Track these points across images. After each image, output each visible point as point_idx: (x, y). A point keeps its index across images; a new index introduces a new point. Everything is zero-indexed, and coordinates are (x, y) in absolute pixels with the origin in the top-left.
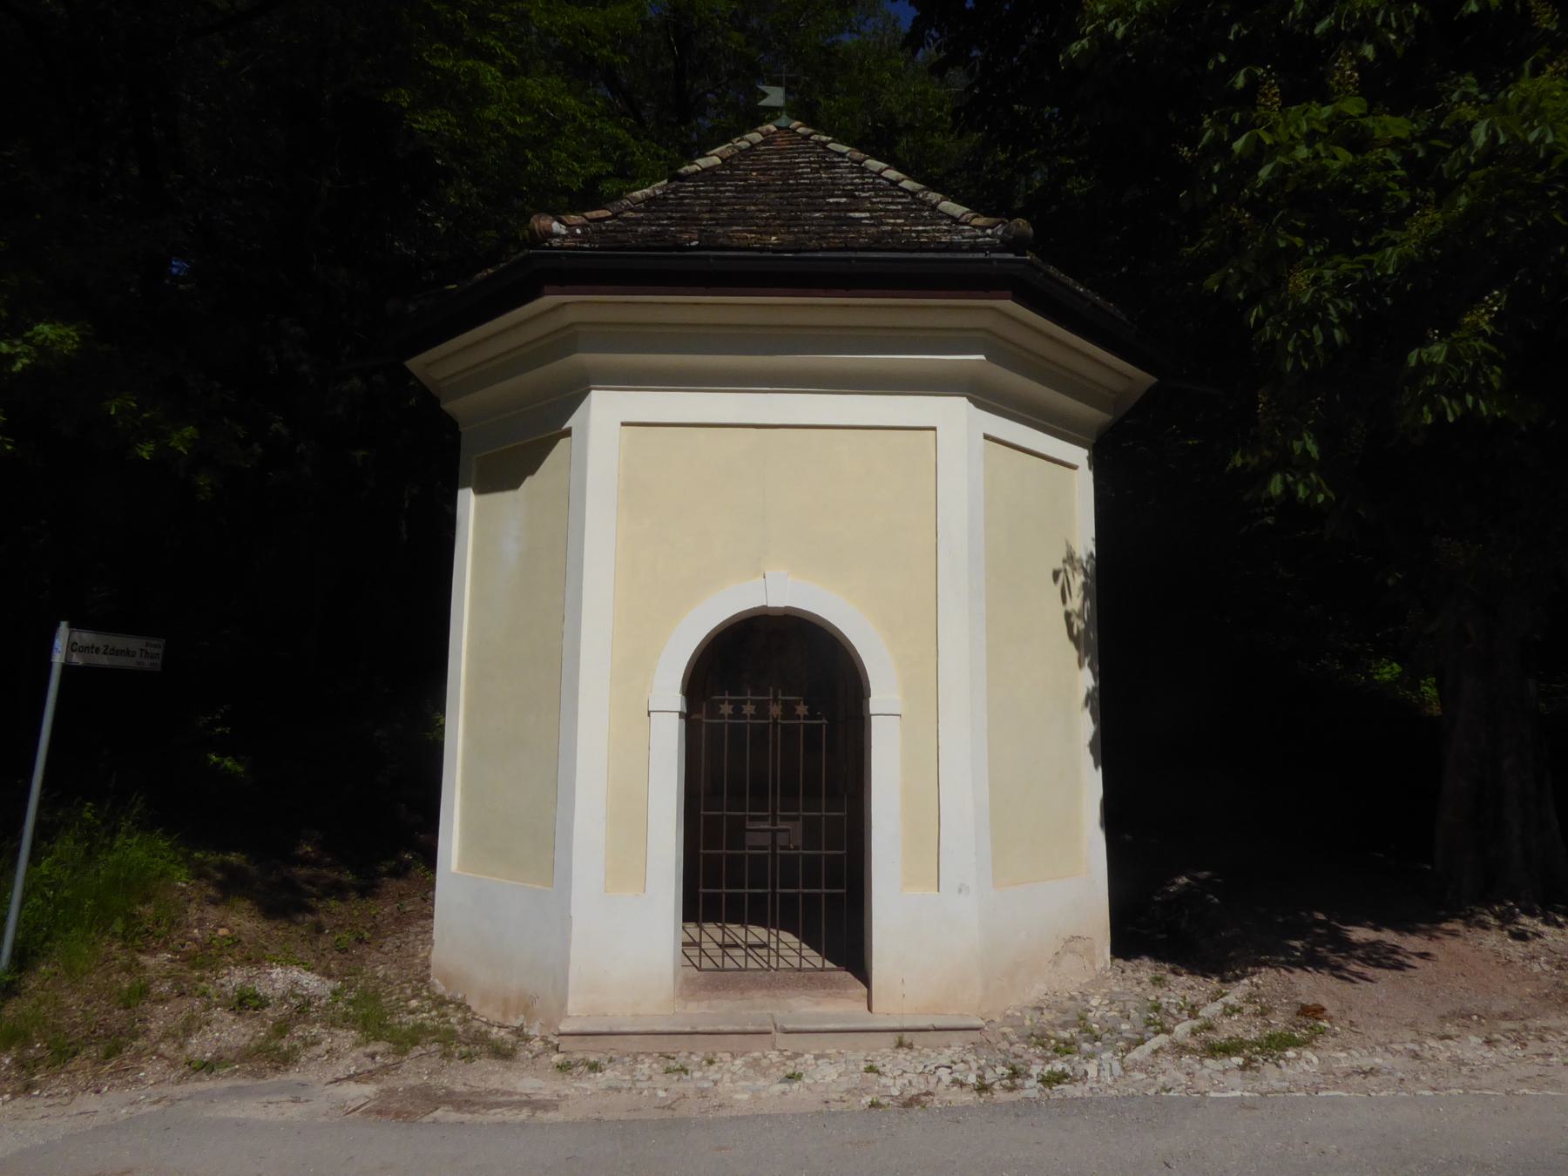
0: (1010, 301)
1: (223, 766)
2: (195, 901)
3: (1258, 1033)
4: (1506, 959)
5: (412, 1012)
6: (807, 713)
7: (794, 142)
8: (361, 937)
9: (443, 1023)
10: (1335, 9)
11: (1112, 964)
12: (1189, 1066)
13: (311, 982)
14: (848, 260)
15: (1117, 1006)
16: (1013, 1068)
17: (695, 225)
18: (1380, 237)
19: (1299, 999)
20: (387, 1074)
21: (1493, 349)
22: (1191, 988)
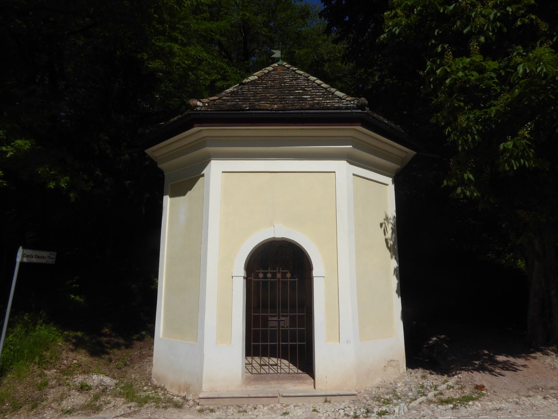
0: (360, 127)
1: (76, 299)
2: (65, 350)
3: (459, 395)
4: (554, 367)
5: (145, 391)
6: (290, 276)
7: (284, 70)
8: (126, 364)
9: (156, 395)
10: (471, 24)
11: (407, 371)
12: (433, 408)
13: (107, 380)
14: (302, 113)
15: (408, 386)
16: (367, 410)
17: (248, 101)
18: (490, 103)
19: (475, 383)
20: (135, 414)
21: (529, 143)
22: (436, 379)
